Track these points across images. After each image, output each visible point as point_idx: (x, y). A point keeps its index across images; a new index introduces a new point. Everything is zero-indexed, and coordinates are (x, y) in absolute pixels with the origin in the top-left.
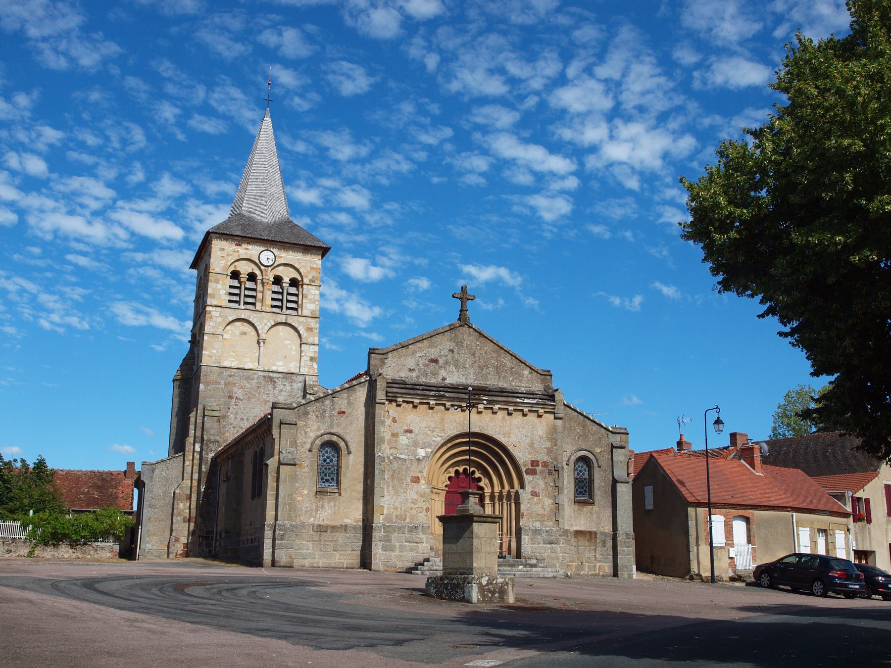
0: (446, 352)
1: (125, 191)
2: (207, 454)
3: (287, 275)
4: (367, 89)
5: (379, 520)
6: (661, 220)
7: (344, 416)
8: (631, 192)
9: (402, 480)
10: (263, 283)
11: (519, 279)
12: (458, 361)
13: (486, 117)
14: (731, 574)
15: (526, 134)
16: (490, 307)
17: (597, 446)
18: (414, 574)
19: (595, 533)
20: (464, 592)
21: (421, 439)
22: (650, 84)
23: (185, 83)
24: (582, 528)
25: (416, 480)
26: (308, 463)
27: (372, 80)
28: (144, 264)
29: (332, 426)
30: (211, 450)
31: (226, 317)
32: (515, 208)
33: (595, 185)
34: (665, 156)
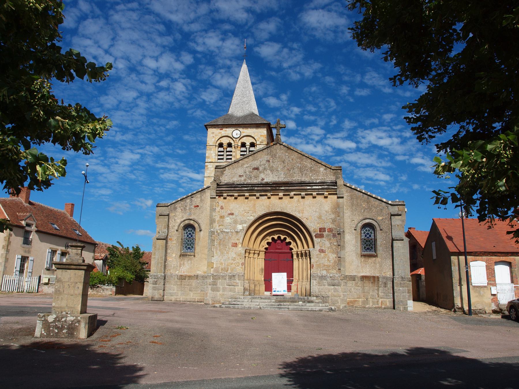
0: (264, 162)
1: (329, 130)
7: (198, 208)
9: (226, 245)
14: (494, 307)
17: (379, 215)
19: (378, 277)
21: (239, 218)
25: (235, 245)
26: (175, 238)
28: (341, 161)
29: (190, 215)
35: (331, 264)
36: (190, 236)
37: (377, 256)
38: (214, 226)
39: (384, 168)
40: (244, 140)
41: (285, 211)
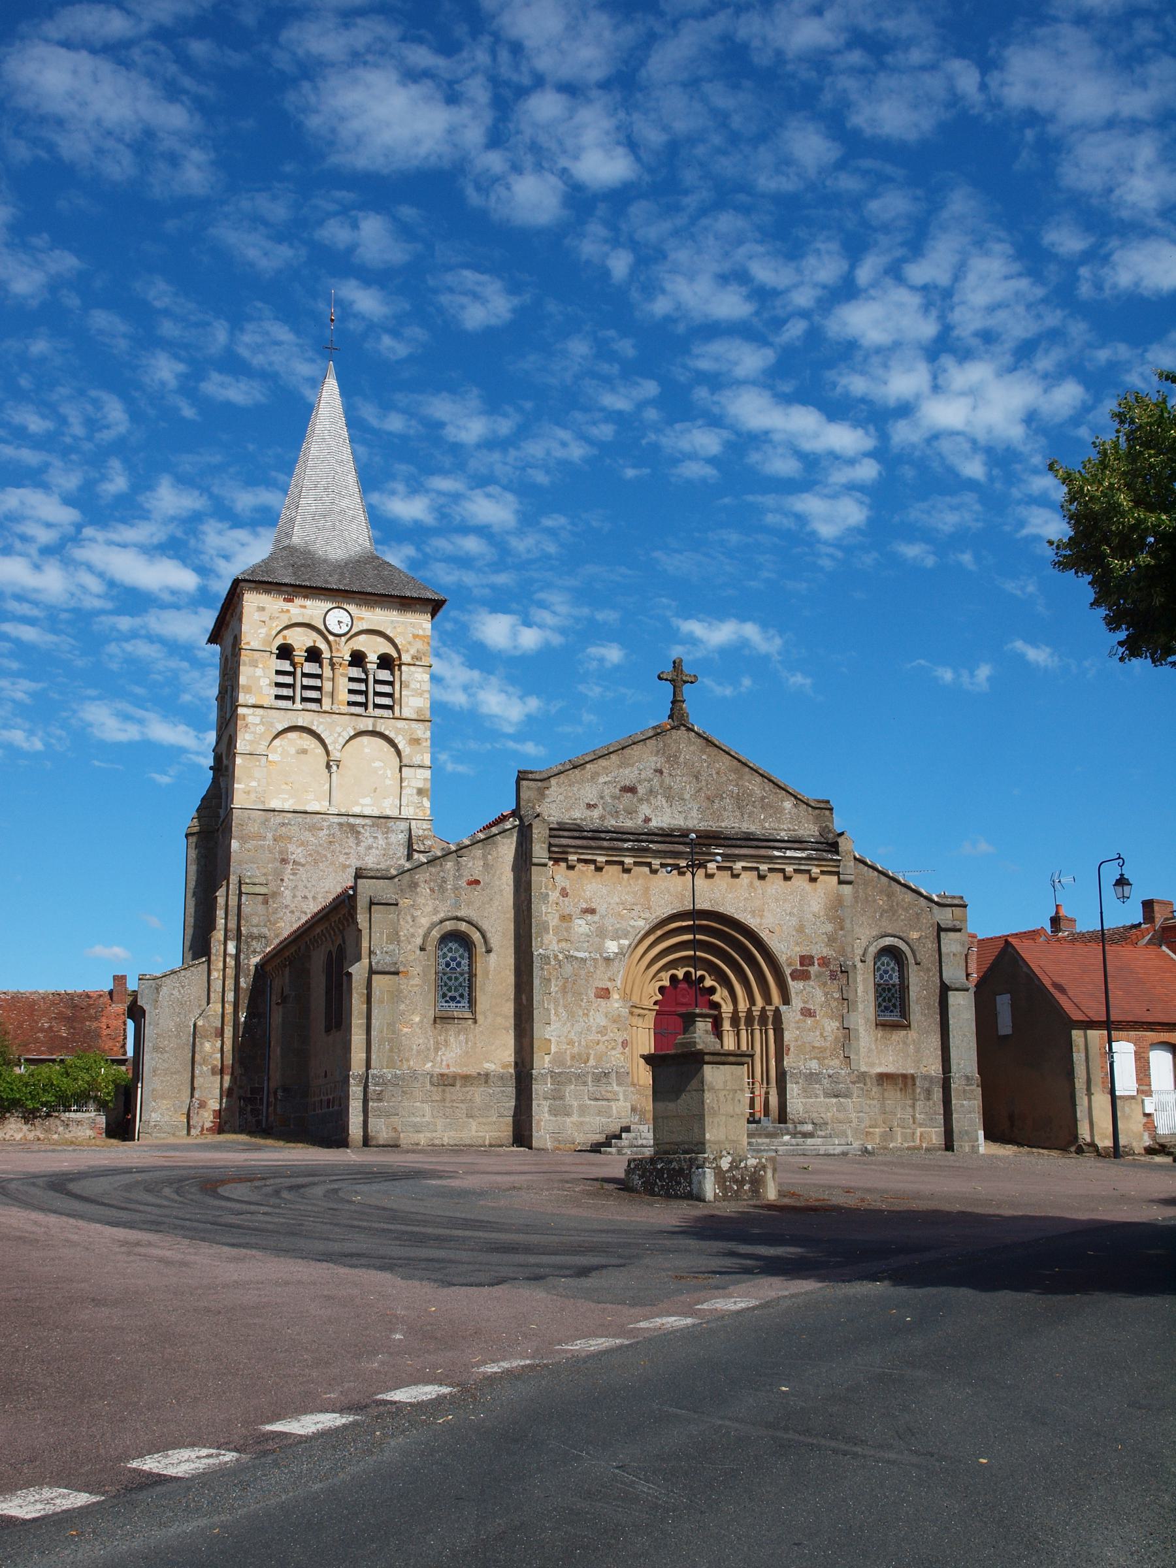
0: (649, 773)
1: (96, 511)
2: (248, 958)
3: (373, 649)
4: (507, 316)
5: (542, 1063)
6: (1025, 532)
7: (479, 888)
8: (971, 485)
9: (581, 994)
10: (332, 665)
11: (778, 641)
12: (670, 788)
13: (717, 359)
14: (1147, 1142)
15: (787, 387)
16: (728, 692)
17: (912, 928)
18: (605, 1153)
19: (913, 1077)
21: (610, 923)
24: (890, 1069)
25: (604, 994)
26: (418, 969)
27: (516, 301)
28: (133, 635)
29: (457, 906)
30: (254, 952)
31: (272, 725)
32: (771, 519)
33: (908, 472)
34: (1031, 418)
35: (828, 1044)
36: (453, 964)
37: (909, 1026)
38: (546, 941)
40: (361, 643)
41: (721, 910)
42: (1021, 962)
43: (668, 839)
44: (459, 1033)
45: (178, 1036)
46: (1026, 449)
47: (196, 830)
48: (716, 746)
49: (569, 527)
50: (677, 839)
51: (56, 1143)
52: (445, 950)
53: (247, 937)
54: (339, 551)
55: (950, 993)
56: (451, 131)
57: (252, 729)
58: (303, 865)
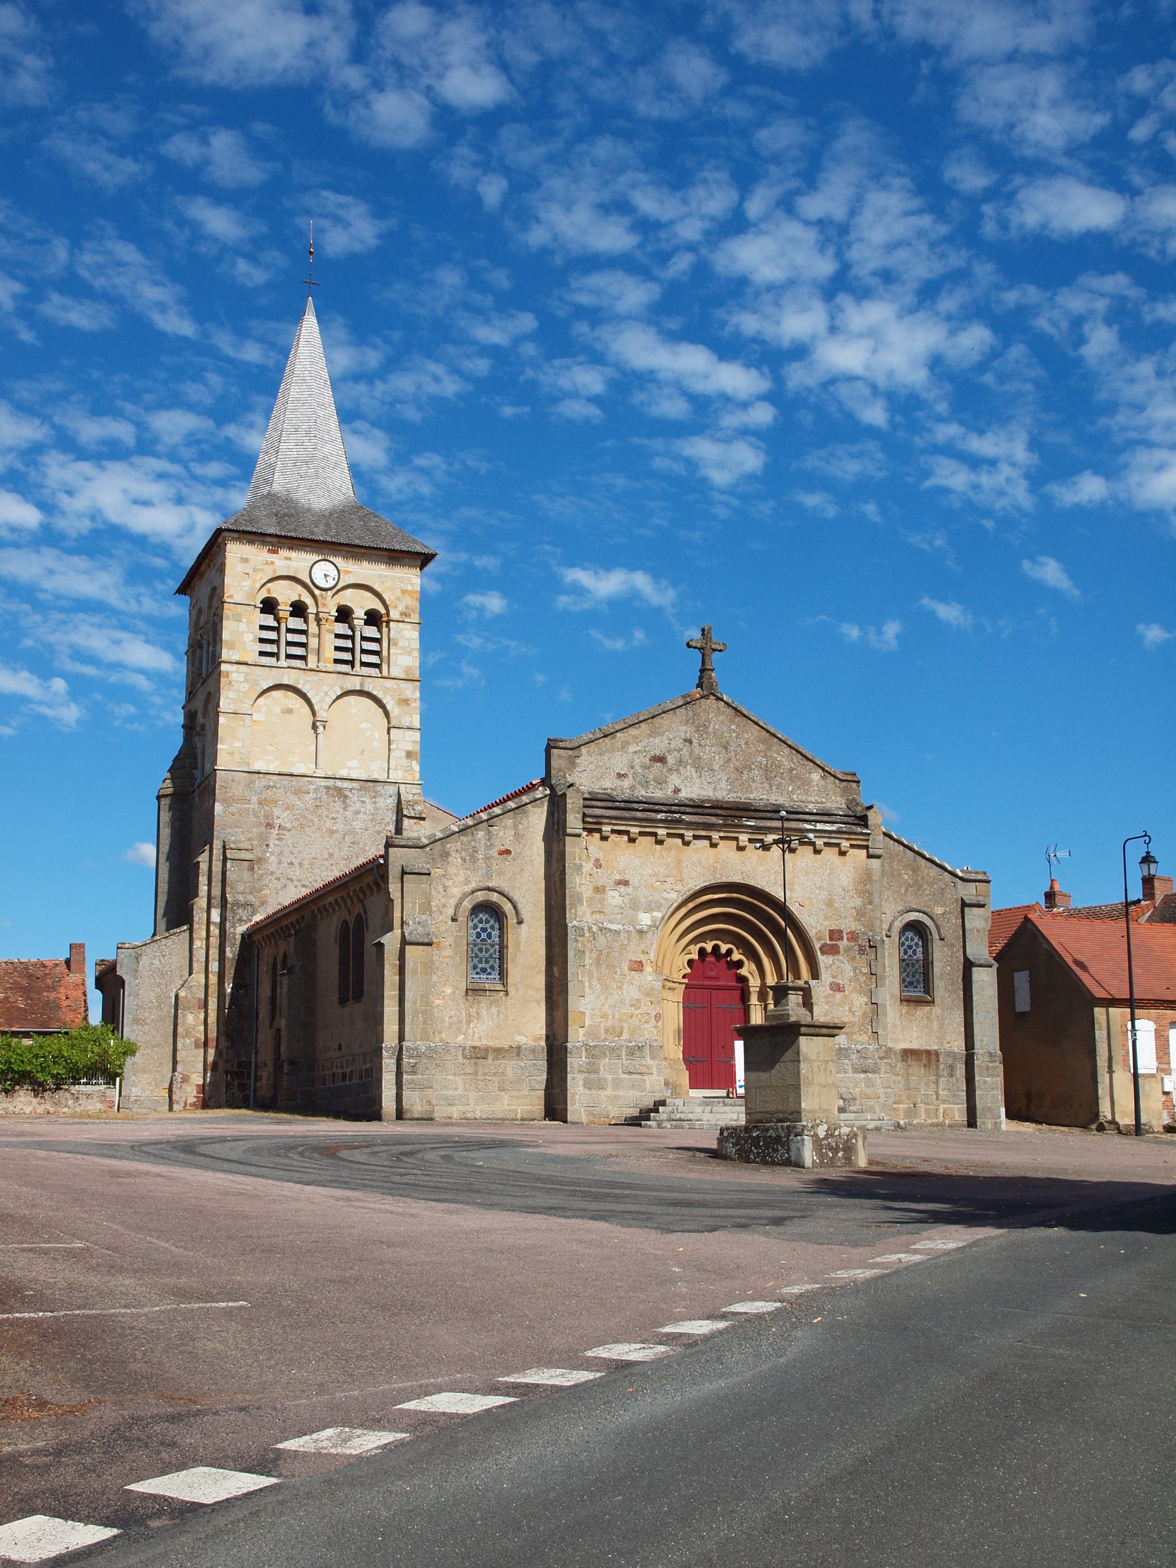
0: (678, 743)
2: (234, 927)
3: (361, 604)
4: (373, 242)
5: (576, 1036)
6: (928, 483)
7: (510, 858)
8: (871, 432)
10: (318, 620)
11: (671, 593)
12: (699, 758)
13: (597, 292)
15: (674, 324)
16: (619, 645)
17: (937, 903)
18: (646, 1126)
19: (937, 1054)
20: (788, 1151)
22: (902, 228)
23: (29, 235)
24: (914, 1045)
25: (638, 967)
26: (450, 940)
27: (383, 226)
29: (489, 876)
30: (241, 920)
31: (256, 683)
32: (658, 463)
33: (807, 418)
34: (935, 363)
35: (856, 1019)
38: (579, 913)
39: (149, 620)
42: (1041, 940)
43: (700, 811)
44: (491, 1005)
45: (159, 1008)
46: (929, 396)
47: (170, 791)
48: (745, 716)
49: (444, 467)
50: (708, 811)
51: (66, 1115)
52: (476, 921)
53: (233, 905)
54: (323, 500)
55: (974, 969)
56: (311, 44)
57: (236, 687)
58: (289, 830)
